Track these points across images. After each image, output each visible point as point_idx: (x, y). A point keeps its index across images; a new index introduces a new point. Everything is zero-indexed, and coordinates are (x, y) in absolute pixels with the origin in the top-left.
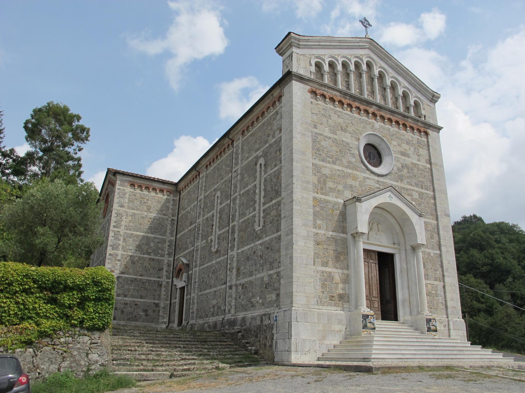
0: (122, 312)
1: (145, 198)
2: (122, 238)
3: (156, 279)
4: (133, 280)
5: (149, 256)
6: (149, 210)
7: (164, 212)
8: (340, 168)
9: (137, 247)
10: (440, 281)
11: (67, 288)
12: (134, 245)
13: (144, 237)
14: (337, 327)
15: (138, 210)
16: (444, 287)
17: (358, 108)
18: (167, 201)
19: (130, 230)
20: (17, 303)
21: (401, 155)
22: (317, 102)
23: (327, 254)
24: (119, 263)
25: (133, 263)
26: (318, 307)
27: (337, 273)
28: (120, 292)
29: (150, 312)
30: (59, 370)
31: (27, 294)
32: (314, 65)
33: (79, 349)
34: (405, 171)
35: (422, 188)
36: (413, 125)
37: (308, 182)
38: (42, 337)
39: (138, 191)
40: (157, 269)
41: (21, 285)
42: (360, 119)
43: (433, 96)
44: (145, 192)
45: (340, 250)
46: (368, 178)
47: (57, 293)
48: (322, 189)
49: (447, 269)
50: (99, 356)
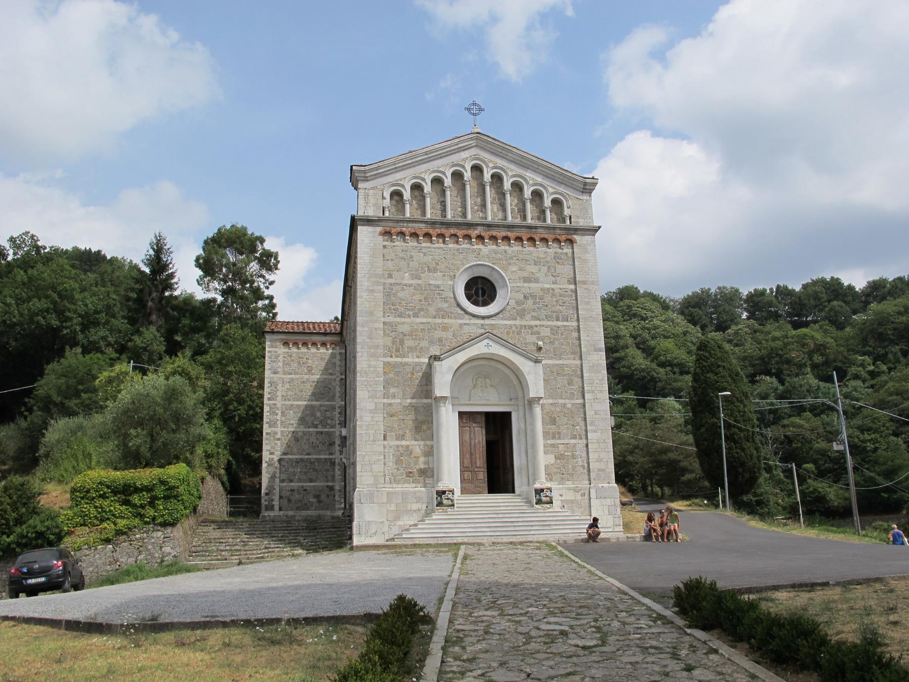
0: (289, 500)
1: (303, 358)
2: (279, 413)
3: (327, 457)
4: (298, 462)
5: (316, 430)
6: (310, 371)
7: (330, 371)
8: (424, 320)
9: (299, 420)
10: (581, 438)
11: (137, 490)
12: (297, 419)
13: (307, 406)
14: (415, 507)
15: (296, 373)
16: (587, 445)
18: (333, 356)
19: (289, 400)
20: (96, 507)
21: (524, 282)
22: (394, 244)
23: (403, 426)
24: (279, 442)
25: (297, 440)
26: (391, 486)
27: (417, 447)
28: (284, 476)
29: (323, 497)
30: (136, 562)
31: (103, 499)
33: (153, 543)
35: (558, 320)
36: (546, 236)
37: (377, 347)
38: (118, 535)
39: (294, 350)
40: (327, 444)
41: (97, 491)
42: (458, 249)
43: (585, 184)
44: (304, 350)
45: (421, 418)
46: (465, 324)
47: (130, 495)
48: (398, 350)
49: (592, 424)
50: (172, 548)
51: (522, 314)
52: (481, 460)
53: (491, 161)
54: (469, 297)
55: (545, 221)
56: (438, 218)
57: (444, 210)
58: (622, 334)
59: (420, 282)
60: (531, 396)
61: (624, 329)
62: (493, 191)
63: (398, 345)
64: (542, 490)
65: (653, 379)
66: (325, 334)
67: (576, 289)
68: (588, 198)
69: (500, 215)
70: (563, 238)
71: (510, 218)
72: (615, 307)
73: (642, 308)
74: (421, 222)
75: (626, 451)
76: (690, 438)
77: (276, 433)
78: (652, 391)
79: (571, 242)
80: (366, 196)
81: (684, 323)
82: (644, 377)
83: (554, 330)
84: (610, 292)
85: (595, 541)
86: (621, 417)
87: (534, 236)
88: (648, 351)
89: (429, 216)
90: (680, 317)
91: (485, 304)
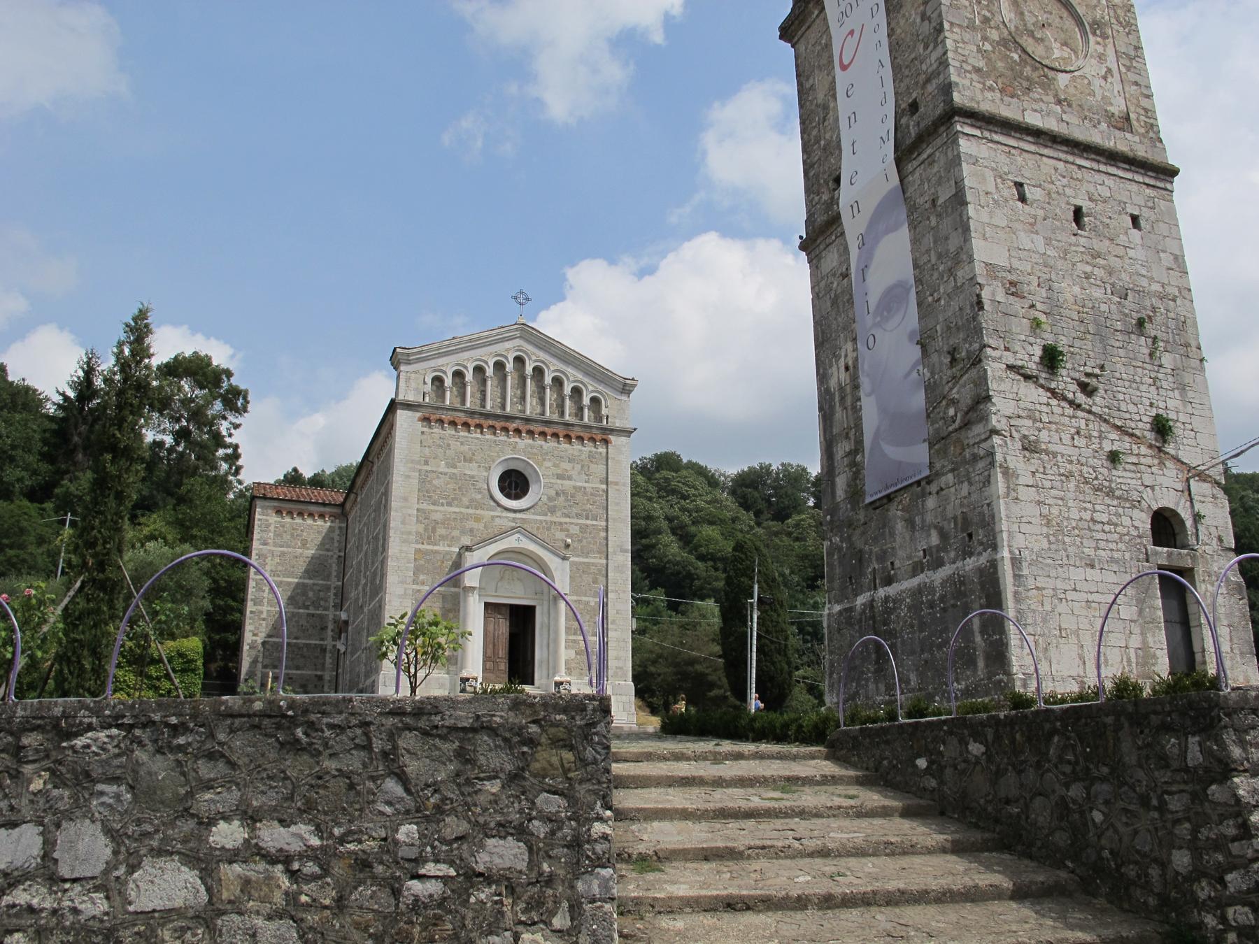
3: (317, 642)
5: (306, 611)
6: (304, 545)
7: (327, 546)
8: (457, 510)
10: (575, 634)
13: (298, 584)
15: (288, 546)
17: (493, 427)
18: (331, 529)
19: (278, 576)
28: (267, 661)
32: (429, 381)
34: (562, 499)
35: (587, 518)
36: (582, 434)
37: (410, 533)
39: (288, 519)
42: (495, 441)
43: (625, 385)
44: (298, 520)
45: (448, 606)
48: (429, 538)
51: (552, 510)
52: (503, 651)
54: (502, 489)
55: (582, 419)
56: (478, 408)
57: (483, 399)
58: (656, 514)
59: (455, 471)
61: (658, 509)
63: (429, 534)
64: (562, 683)
65: (690, 576)
66: (324, 504)
68: (626, 398)
69: (538, 410)
70: (599, 437)
71: (548, 413)
72: (649, 479)
74: (461, 411)
75: (648, 660)
76: (717, 649)
77: (262, 612)
78: (687, 590)
79: (606, 442)
80: (407, 380)
81: (735, 506)
82: (679, 573)
86: (645, 620)
87: (571, 434)
88: (686, 539)
89: (468, 405)
90: (730, 498)
91: (517, 497)
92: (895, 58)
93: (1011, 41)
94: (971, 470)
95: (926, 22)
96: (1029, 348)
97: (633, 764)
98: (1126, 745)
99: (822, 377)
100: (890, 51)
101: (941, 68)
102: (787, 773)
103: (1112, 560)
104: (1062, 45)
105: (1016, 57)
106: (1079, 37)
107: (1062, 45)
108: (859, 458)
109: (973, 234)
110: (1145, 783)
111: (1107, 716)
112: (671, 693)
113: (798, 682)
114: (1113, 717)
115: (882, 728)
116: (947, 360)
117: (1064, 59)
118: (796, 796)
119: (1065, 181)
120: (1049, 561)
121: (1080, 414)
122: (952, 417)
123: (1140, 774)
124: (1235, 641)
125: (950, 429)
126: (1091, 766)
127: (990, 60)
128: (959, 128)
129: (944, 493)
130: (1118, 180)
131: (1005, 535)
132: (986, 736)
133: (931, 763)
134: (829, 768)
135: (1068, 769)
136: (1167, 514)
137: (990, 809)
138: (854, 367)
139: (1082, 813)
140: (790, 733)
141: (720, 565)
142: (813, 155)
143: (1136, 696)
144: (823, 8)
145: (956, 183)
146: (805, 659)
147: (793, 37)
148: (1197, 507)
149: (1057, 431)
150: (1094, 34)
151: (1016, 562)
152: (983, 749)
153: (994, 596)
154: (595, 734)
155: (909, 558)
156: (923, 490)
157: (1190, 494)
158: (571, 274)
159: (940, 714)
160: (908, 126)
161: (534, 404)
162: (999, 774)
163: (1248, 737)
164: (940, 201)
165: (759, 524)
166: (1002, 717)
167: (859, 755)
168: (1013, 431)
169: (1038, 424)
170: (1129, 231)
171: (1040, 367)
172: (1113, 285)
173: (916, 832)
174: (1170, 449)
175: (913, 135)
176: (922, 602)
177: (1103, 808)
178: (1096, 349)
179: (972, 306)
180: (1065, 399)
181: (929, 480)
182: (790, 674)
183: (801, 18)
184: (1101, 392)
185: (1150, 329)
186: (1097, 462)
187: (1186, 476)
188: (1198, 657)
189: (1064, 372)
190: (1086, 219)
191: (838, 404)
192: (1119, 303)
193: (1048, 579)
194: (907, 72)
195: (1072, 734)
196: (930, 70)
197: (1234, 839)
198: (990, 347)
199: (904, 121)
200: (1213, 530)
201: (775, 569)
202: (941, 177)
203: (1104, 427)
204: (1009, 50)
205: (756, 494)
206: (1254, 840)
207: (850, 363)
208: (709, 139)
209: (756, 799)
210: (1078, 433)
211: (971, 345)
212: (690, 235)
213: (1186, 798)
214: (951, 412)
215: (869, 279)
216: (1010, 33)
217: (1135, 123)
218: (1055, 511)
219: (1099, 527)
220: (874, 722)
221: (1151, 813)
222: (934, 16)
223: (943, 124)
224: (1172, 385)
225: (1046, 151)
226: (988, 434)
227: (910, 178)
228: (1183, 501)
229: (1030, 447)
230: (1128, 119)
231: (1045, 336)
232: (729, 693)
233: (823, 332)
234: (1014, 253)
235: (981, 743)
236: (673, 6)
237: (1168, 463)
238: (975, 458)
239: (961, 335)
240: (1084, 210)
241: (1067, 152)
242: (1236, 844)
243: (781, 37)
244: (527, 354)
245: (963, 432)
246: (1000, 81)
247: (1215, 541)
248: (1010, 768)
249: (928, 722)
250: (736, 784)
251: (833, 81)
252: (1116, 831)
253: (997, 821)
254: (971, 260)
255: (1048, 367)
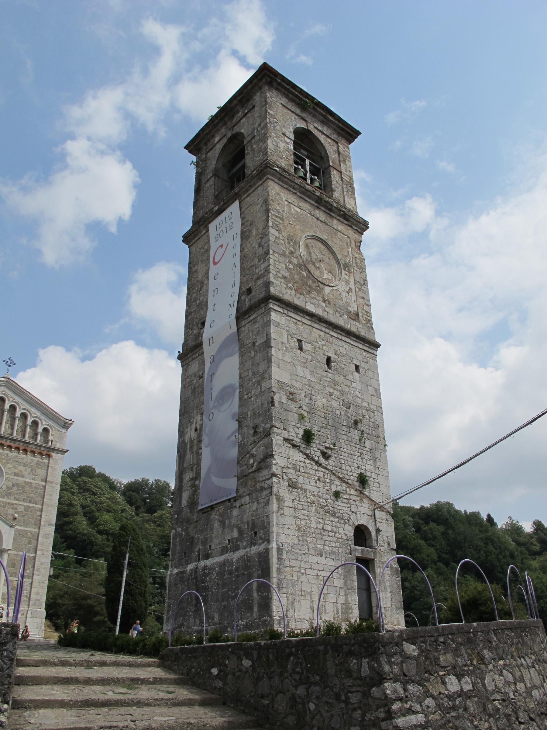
10: (29, 578)
16: (32, 583)
34: (15, 489)
35: (30, 502)
36: (34, 450)
43: (66, 423)
49: (38, 570)
51: (9, 495)
53: (12, 397)
55: (36, 440)
60: (4, 547)
62: (9, 415)
65: (91, 543)
67: (45, 486)
69: (9, 431)
71: (15, 435)
72: (74, 481)
73: (94, 486)
76: (103, 590)
79: (49, 456)
82: (85, 540)
83: (27, 509)
84: (73, 468)
85: (25, 640)
86: (60, 569)
87: (27, 449)
88: (92, 519)
90: (122, 497)
92: (243, 264)
93: (303, 266)
94: (259, 495)
95: (261, 248)
96: (297, 430)
97: (33, 668)
98: (329, 664)
99: (181, 433)
100: (241, 259)
101: (266, 273)
102: (133, 676)
103: (332, 553)
104: (329, 272)
105: (305, 274)
106: (337, 269)
107: (329, 272)
108: (197, 482)
109: (273, 364)
110: (338, 686)
111: (320, 645)
112: (71, 616)
113: (151, 614)
114: (323, 646)
115: (193, 648)
116: (252, 432)
117: (329, 279)
118: (136, 691)
119: (323, 342)
120: (298, 551)
121: (321, 469)
122: (251, 464)
123: (336, 681)
124: (393, 601)
125: (250, 471)
126: (310, 675)
127: (291, 273)
128: (271, 306)
129: (243, 507)
130: (350, 346)
131: (275, 534)
132: (253, 655)
133: (220, 671)
134: (159, 673)
135: (297, 677)
136: (363, 528)
137: (252, 701)
138: (200, 430)
139: (303, 704)
140: (138, 649)
141: (111, 538)
142: (192, 307)
143: (337, 634)
144: (208, 230)
145: (267, 335)
146: (156, 599)
147: (190, 242)
148: (378, 525)
149: (308, 478)
150: (345, 270)
151: (280, 550)
152: (250, 663)
153: (266, 572)
154: (5, 650)
155: (220, 544)
156: (232, 504)
157: (375, 518)
158: (42, 352)
159: (228, 641)
160: (245, 300)
161: (7, 427)
162: (258, 679)
163: (393, 660)
164: (257, 344)
165: (137, 515)
166: (263, 644)
167: (178, 665)
168: (284, 475)
169: (298, 473)
170: (354, 373)
171: (302, 441)
172: (343, 400)
173: (207, 716)
174: (366, 492)
175: (247, 306)
176: (225, 571)
177: (315, 701)
178: (332, 434)
179: (268, 403)
180: (313, 460)
181: (235, 499)
182: (146, 609)
183: (195, 233)
184: (333, 458)
185: (360, 426)
186: (327, 497)
187: (373, 508)
188: (374, 609)
189: (314, 445)
190: (332, 364)
191: (188, 450)
192: (346, 410)
193: (296, 561)
194: (248, 272)
195: (301, 656)
196: (260, 273)
197: (384, 720)
198: (275, 427)
199: (243, 297)
200: (385, 538)
201: (143, 543)
202: (259, 331)
203: (333, 477)
204: (302, 270)
205: (138, 497)
206: (393, 720)
207: (198, 427)
208: (134, 289)
209: (110, 693)
210: (319, 479)
211: (265, 424)
212: (117, 340)
213: (360, 695)
214: (251, 461)
215: (214, 381)
216: (303, 262)
217: (361, 318)
218: (303, 522)
219: (326, 533)
220: (189, 644)
221: (341, 704)
222: (266, 245)
223: (263, 303)
224: (369, 457)
225: (316, 325)
226: (270, 476)
227: (243, 329)
228: (371, 521)
229: (292, 485)
230: (357, 315)
231: (306, 424)
232: (106, 619)
233: (185, 407)
234: (293, 377)
235: (250, 660)
236: (125, 215)
237: (365, 500)
238: (262, 489)
239: (261, 419)
240: (332, 359)
241: (326, 328)
242: (384, 723)
243: (183, 241)
244: (8, 397)
245: (256, 473)
246: (295, 285)
247: (386, 545)
248: (265, 676)
249: (220, 645)
250: (99, 682)
251: (208, 270)
252: (321, 715)
253: (256, 709)
254: (270, 378)
255: (306, 442)
